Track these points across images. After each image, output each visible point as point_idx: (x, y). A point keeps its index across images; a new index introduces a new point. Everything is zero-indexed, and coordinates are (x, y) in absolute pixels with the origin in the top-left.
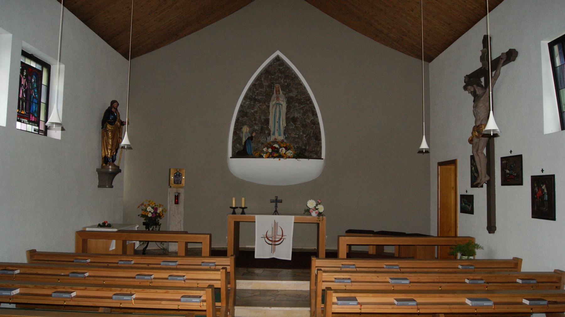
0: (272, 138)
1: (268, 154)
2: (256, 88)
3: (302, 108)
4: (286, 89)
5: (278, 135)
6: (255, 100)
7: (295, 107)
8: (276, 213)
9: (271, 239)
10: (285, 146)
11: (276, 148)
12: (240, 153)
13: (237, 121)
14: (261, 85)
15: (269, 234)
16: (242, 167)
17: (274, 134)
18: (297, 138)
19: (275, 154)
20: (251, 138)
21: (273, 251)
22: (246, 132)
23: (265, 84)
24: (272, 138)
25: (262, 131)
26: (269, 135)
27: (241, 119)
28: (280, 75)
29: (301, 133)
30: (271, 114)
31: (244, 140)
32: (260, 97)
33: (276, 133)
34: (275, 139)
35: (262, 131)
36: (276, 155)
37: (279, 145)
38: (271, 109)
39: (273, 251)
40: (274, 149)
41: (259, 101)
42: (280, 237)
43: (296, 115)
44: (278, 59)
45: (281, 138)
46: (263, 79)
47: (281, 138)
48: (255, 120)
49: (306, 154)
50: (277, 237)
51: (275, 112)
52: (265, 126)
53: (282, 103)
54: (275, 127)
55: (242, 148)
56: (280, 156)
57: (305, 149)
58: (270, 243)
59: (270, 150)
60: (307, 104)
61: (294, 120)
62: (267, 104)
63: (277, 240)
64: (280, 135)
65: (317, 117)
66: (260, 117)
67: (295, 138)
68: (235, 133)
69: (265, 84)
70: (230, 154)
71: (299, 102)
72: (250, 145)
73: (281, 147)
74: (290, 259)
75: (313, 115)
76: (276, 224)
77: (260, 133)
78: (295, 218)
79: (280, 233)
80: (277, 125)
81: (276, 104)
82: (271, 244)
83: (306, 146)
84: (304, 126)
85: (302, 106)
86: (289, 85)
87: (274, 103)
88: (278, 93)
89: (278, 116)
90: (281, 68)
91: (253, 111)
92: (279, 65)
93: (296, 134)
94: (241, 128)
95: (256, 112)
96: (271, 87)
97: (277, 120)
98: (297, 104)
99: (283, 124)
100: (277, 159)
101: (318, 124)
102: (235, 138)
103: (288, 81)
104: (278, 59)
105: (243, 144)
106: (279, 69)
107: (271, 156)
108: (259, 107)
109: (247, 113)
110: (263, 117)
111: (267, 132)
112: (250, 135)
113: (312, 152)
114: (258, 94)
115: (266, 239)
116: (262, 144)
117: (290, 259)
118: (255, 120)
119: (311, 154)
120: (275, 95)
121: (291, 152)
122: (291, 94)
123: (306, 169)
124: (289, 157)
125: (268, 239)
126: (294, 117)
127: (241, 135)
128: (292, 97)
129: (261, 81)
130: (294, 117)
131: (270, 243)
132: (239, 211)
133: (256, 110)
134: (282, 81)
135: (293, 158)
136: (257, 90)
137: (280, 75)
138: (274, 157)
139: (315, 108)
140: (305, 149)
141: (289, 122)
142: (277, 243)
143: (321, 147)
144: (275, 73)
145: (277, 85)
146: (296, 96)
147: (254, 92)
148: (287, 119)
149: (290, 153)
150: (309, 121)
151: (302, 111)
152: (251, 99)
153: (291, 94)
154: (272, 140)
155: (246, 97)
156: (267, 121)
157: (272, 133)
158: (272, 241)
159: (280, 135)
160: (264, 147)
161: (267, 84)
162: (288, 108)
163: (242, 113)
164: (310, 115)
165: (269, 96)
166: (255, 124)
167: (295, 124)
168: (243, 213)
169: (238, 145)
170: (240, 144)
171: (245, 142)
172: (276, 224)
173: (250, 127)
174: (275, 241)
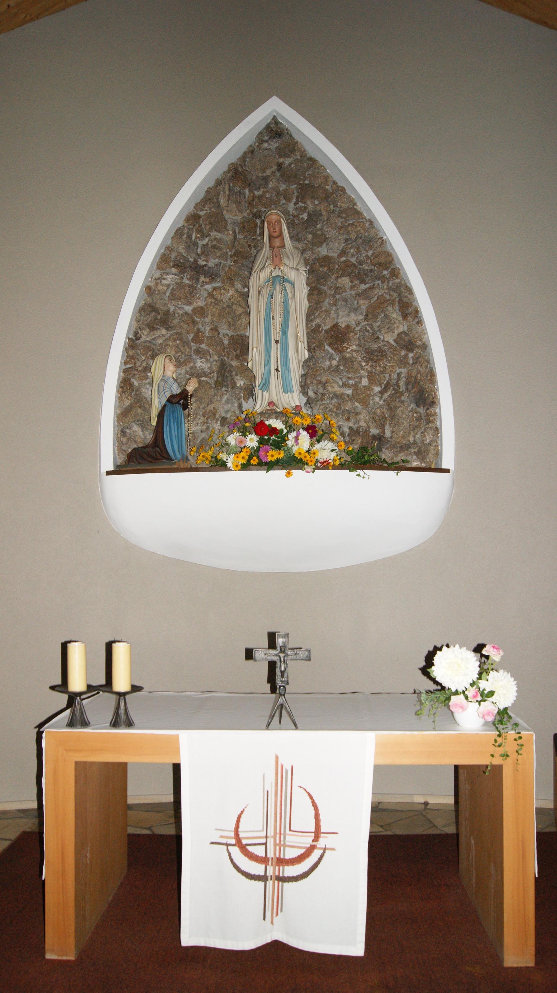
0: (259, 404)
1: (245, 454)
2: (200, 231)
3: (364, 295)
4: (306, 230)
5: (280, 391)
6: (198, 270)
7: (338, 290)
8: (280, 714)
9: (259, 851)
10: (308, 422)
11: (274, 431)
12: (146, 456)
13: (132, 343)
14: (217, 221)
15: (252, 828)
16: (161, 509)
17: (266, 386)
18: (352, 398)
19: (271, 450)
20: (181, 400)
21: (272, 907)
22: (164, 380)
23: (233, 216)
24: (259, 404)
25: (224, 377)
26: (250, 392)
27: (145, 336)
28: (283, 187)
29: (365, 382)
30: (253, 313)
31: (156, 406)
32: (212, 262)
33: (275, 384)
34: (271, 403)
35: (224, 377)
36: (273, 455)
37: (286, 423)
38: (252, 299)
39: (272, 907)
40: (262, 429)
41: (212, 275)
42: (308, 841)
43: (345, 319)
44: (274, 130)
45: (294, 399)
46: (222, 201)
47: (294, 399)
48: (197, 339)
49: (386, 455)
50: (290, 839)
51: (270, 309)
52: (235, 363)
53: (291, 275)
54: (268, 363)
55: (149, 437)
56: (292, 463)
57: (380, 438)
58: (257, 869)
59: (252, 440)
60: (382, 278)
61: (338, 337)
62: (239, 286)
63: (291, 854)
64: (287, 389)
65: (420, 322)
66: (215, 329)
67: (340, 396)
68: (125, 385)
69: (228, 216)
70: (107, 461)
71: (351, 270)
72: (179, 426)
73: (291, 428)
74: (357, 949)
75: (405, 317)
76: (283, 777)
77: (219, 384)
78: (380, 747)
79: (303, 819)
80: (276, 352)
81: (273, 280)
82: (263, 878)
83: (382, 427)
84: (374, 356)
85: (363, 287)
86: (314, 217)
87: (264, 275)
88: (277, 242)
89: (278, 322)
90: (287, 161)
91: (189, 309)
92: (280, 152)
93: (345, 385)
94: (148, 369)
95: (201, 311)
96: (251, 227)
97: (276, 334)
98: (345, 281)
99: (298, 352)
100: (278, 474)
101: (425, 347)
102: (127, 403)
103: (311, 207)
104: (274, 130)
105: (154, 423)
106: (280, 166)
107: (255, 462)
108: (210, 295)
109: (167, 313)
110: (225, 330)
111: (240, 382)
112: (176, 390)
113: (405, 447)
114: (206, 251)
115: (236, 852)
116: (224, 420)
117: (357, 949)
118: (197, 339)
119: (402, 456)
120: (266, 250)
121: (331, 445)
122: (323, 251)
123: (391, 509)
124: (325, 465)
125: (244, 849)
126: (335, 326)
127: (146, 392)
128: (326, 260)
129: (218, 206)
130: (335, 326)
131: (257, 869)
132: (99, 708)
133: (201, 303)
134: (291, 207)
135: (341, 467)
136: (203, 236)
137: (283, 187)
138: (270, 466)
139: (410, 291)
140: (380, 438)
141: (320, 346)
142: (290, 871)
143: (437, 431)
144: (266, 179)
145: (274, 215)
146: (343, 253)
147: (191, 245)
148: (313, 333)
149: (326, 450)
150: (390, 338)
151: (364, 304)
152: (181, 266)
153: (323, 251)
154: (259, 408)
155: (164, 260)
156: (241, 346)
157: (258, 381)
158: (264, 860)
159: (287, 389)
160: (231, 432)
161: (239, 218)
162: (315, 292)
163: (151, 314)
164: (395, 314)
165: (245, 259)
166: (198, 352)
167: (340, 351)
168: (122, 719)
169: (136, 428)
170: (144, 424)
171: (161, 416)
172: (283, 777)
173: (179, 364)
174: (281, 862)
